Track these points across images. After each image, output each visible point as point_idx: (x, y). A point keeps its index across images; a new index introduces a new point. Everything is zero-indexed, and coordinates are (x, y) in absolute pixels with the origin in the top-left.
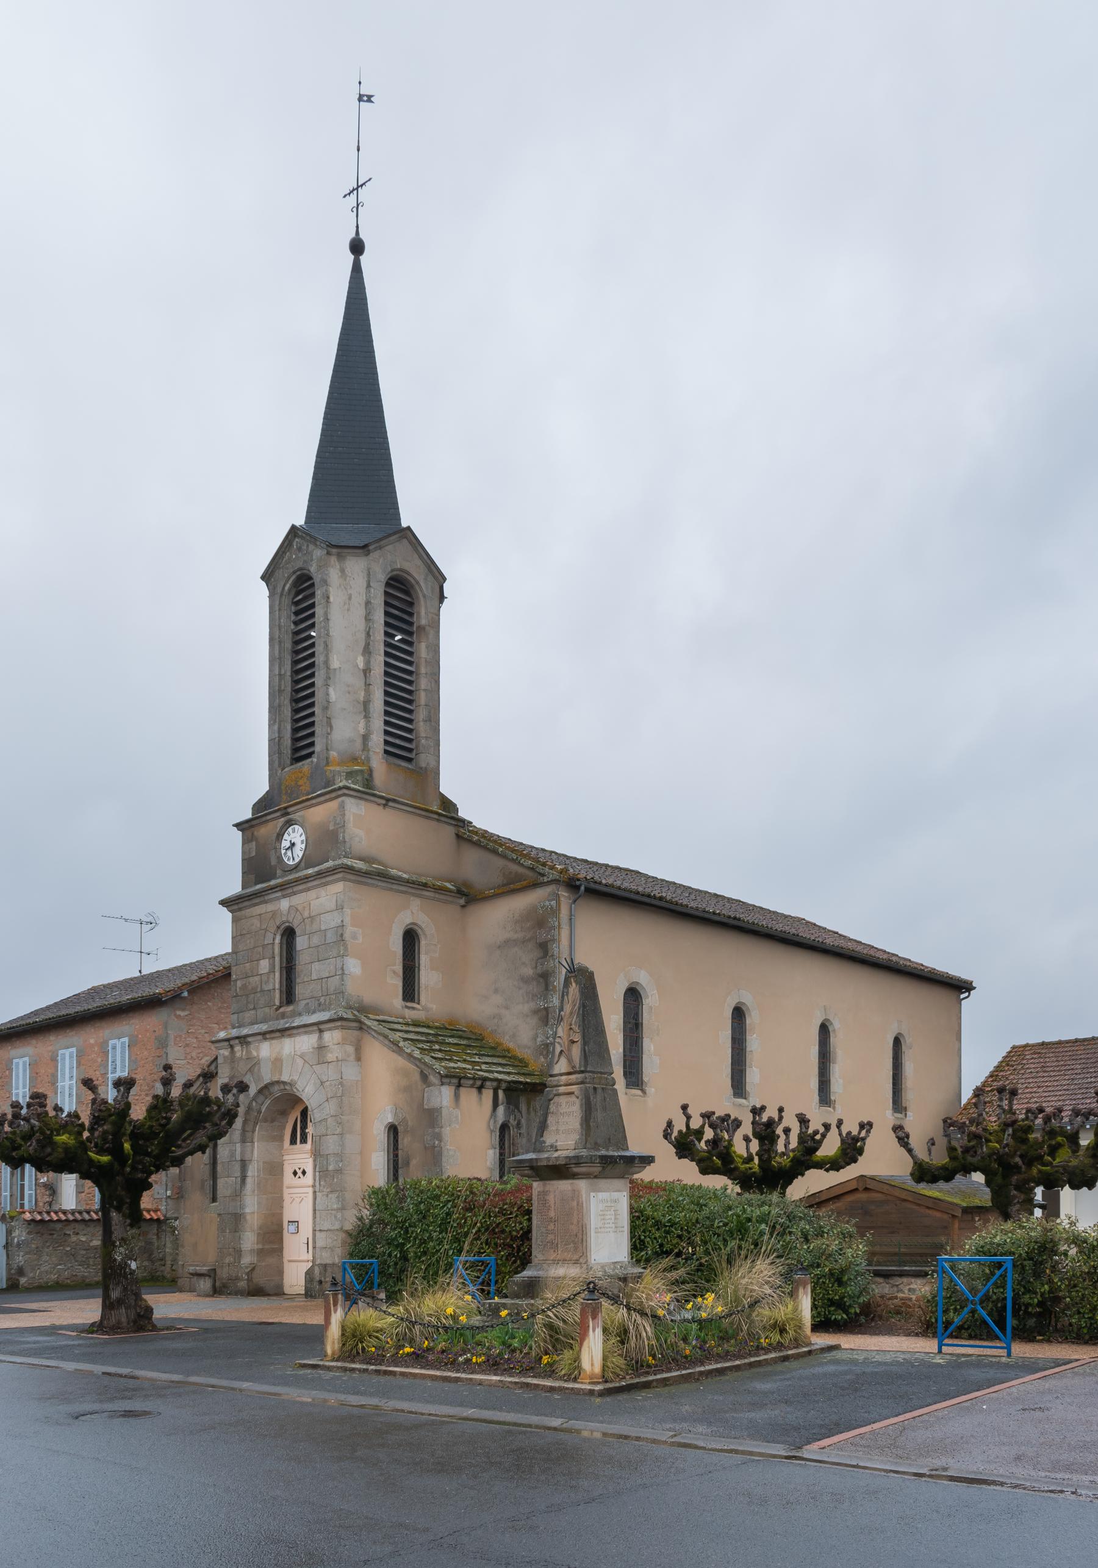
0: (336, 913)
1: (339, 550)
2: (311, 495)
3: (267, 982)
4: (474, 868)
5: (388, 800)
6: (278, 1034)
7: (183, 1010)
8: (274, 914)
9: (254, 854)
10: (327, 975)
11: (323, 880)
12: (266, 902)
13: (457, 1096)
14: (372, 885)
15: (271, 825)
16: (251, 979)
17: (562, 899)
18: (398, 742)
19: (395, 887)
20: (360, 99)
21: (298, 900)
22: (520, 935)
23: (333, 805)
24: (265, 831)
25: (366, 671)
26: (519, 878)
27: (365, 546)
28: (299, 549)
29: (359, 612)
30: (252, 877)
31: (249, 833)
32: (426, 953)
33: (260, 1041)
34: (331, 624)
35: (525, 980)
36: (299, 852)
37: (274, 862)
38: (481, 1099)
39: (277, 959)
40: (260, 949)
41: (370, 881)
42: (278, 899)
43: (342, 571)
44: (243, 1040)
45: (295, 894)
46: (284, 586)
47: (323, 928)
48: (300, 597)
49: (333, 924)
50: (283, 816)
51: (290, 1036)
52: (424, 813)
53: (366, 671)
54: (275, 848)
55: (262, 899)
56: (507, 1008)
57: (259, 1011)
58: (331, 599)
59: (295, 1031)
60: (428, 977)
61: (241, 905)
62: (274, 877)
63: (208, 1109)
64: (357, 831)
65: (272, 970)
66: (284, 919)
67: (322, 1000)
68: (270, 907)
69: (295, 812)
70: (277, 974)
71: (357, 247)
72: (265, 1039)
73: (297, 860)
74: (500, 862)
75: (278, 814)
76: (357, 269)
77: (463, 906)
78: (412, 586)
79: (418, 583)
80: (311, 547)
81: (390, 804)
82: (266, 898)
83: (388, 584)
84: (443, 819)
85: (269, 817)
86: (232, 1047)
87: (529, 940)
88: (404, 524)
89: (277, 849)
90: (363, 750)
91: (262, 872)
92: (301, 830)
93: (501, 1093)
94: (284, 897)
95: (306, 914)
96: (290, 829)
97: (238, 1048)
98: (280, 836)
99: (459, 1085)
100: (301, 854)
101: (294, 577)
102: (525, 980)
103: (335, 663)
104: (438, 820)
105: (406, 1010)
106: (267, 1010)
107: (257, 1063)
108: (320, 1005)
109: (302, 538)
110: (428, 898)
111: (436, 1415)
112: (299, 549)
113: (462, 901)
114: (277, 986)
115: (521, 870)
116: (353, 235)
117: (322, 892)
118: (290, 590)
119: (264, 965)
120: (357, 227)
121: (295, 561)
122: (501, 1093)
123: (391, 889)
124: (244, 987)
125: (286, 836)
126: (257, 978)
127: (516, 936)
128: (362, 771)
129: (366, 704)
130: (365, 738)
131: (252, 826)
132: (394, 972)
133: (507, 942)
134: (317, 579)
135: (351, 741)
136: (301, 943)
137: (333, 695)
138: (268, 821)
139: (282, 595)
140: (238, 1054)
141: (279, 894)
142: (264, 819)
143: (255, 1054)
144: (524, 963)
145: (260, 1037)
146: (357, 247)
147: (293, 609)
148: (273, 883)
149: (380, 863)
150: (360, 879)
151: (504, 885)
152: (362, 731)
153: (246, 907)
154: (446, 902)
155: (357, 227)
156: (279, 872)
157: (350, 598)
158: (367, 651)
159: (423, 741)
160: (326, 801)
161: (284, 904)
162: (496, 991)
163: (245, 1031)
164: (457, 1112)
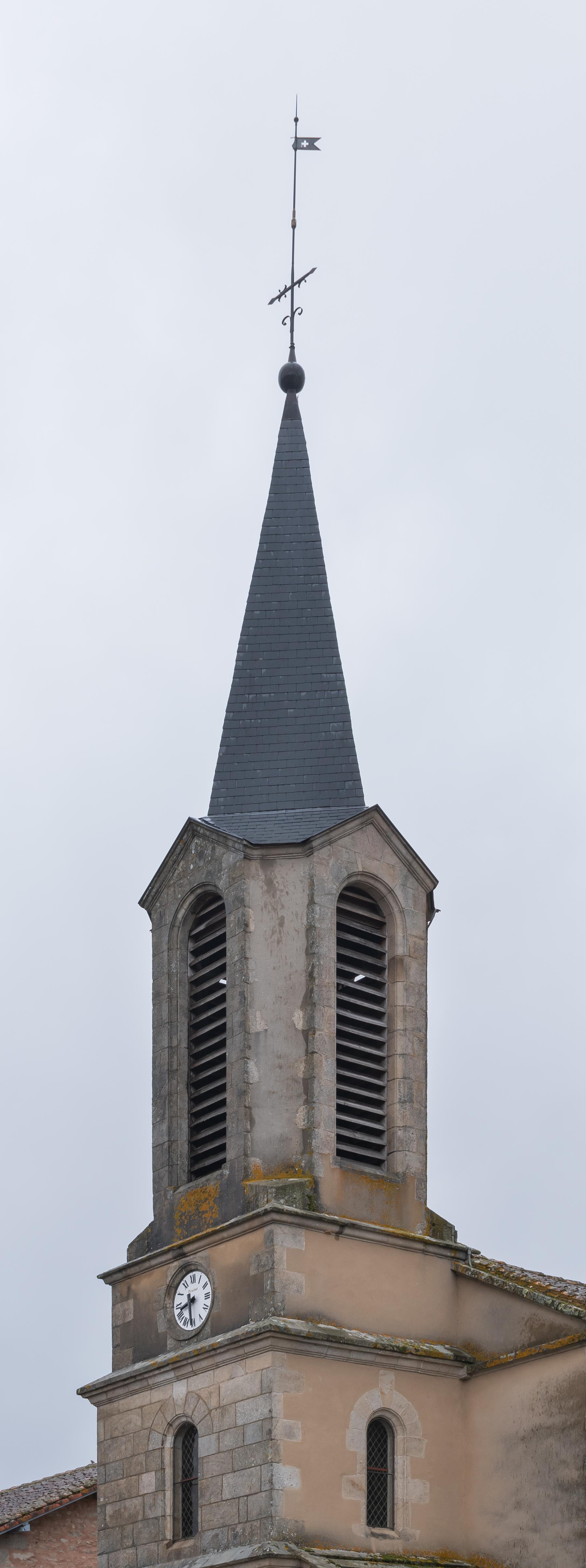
0: (260, 1400)
1: (264, 852)
3: (153, 1505)
4: (482, 1320)
5: (343, 1226)
7: (24, 1551)
8: (163, 1405)
9: (130, 1317)
10: (248, 1492)
11: (241, 1352)
12: (150, 1388)
15: (157, 1273)
16: (128, 1503)
18: (359, 1136)
19: (354, 1356)
20: (297, 146)
21: (200, 1383)
22: (557, 1420)
23: (257, 1238)
24: (148, 1284)
25: (308, 1033)
26: (556, 1332)
28: (200, 855)
29: (296, 944)
30: (129, 1352)
31: (123, 1287)
32: (405, 1453)
34: (251, 964)
35: (566, 1487)
36: (200, 1312)
37: (162, 1328)
39: (169, 1471)
40: (142, 1458)
41: (314, 1349)
42: (170, 1382)
43: (269, 883)
45: (195, 1373)
46: (177, 912)
47: (240, 1422)
48: (202, 927)
49: (256, 1416)
50: (176, 1258)
53: (308, 1033)
54: (165, 1308)
55: (144, 1383)
56: (535, 1530)
57: (140, 1550)
58: (252, 927)
60: (408, 1488)
61: (110, 1395)
62: (163, 1350)
65: (160, 1488)
66: (179, 1411)
67: (239, 1529)
68: (157, 1395)
69: (194, 1252)
70: (169, 1494)
71: (292, 379)
73: (198, 1323)
74: (525, 1311)
75: (169, 1256)
76: (291, 413)
77: (464, 1380)
78: (383, 897)
79: (391, 891)
80: (219, 850)
81: (347, 1231)
82: (151, 1382)
84: (431, 1249)
85: (154, 1262)
87: (573, 1426)
89: (167, 1309)
90: (303, 1153)
91: (142, 1341)
92: (204, 1279)
94: (178, 1379)
95: (213, 1403)
96: (188, 1278)
98: (172, 1289)
100: (204, 1314)
101: (192, 898)
102: (566, 1487)
103: (257, 1024)
104: (424, 1252)
105: (373, 1539)
106: (153, 1547)
108: (235, 1536)
109: (204, 837)
112: (200, 855)
113: (463, 1372)
114: (169, 1511)
115: (559, 1320)
116: (285, 361)
117: (239, 1369)
118: (185, 918)
119: (148, 1481)
120: (292, 347)
121: (193, 873)
123: (348, 1360)
124: (117, 1514)
125: (181, 1289)
126: (137, 1501)
127: (549, 1422)
128: (301, 1185)
129: (308, 1083)
130: (307, 1134)
132: (353, 1484)
133: (536, 1431)
134: (228, 899)
136: (205, 1445)
137: (255, 1072)
139: (173, 926)
141: (171, 1375)
144: (564, 1462)
146: (292, 379)
147: (191, 946)
148: (161, 1359)
149: (330, 1321)
151: (531, 1345)
152: (301, 1123)
153: (118, 1398)
154: (437, 1374)
155: (292, 347)
156: (170, 1343)
157: (281, 924)
158: (309, 1002)
159: (400, 1133)
160: (244, 1233)
161: (179, 1390)
162: (518, 1505)
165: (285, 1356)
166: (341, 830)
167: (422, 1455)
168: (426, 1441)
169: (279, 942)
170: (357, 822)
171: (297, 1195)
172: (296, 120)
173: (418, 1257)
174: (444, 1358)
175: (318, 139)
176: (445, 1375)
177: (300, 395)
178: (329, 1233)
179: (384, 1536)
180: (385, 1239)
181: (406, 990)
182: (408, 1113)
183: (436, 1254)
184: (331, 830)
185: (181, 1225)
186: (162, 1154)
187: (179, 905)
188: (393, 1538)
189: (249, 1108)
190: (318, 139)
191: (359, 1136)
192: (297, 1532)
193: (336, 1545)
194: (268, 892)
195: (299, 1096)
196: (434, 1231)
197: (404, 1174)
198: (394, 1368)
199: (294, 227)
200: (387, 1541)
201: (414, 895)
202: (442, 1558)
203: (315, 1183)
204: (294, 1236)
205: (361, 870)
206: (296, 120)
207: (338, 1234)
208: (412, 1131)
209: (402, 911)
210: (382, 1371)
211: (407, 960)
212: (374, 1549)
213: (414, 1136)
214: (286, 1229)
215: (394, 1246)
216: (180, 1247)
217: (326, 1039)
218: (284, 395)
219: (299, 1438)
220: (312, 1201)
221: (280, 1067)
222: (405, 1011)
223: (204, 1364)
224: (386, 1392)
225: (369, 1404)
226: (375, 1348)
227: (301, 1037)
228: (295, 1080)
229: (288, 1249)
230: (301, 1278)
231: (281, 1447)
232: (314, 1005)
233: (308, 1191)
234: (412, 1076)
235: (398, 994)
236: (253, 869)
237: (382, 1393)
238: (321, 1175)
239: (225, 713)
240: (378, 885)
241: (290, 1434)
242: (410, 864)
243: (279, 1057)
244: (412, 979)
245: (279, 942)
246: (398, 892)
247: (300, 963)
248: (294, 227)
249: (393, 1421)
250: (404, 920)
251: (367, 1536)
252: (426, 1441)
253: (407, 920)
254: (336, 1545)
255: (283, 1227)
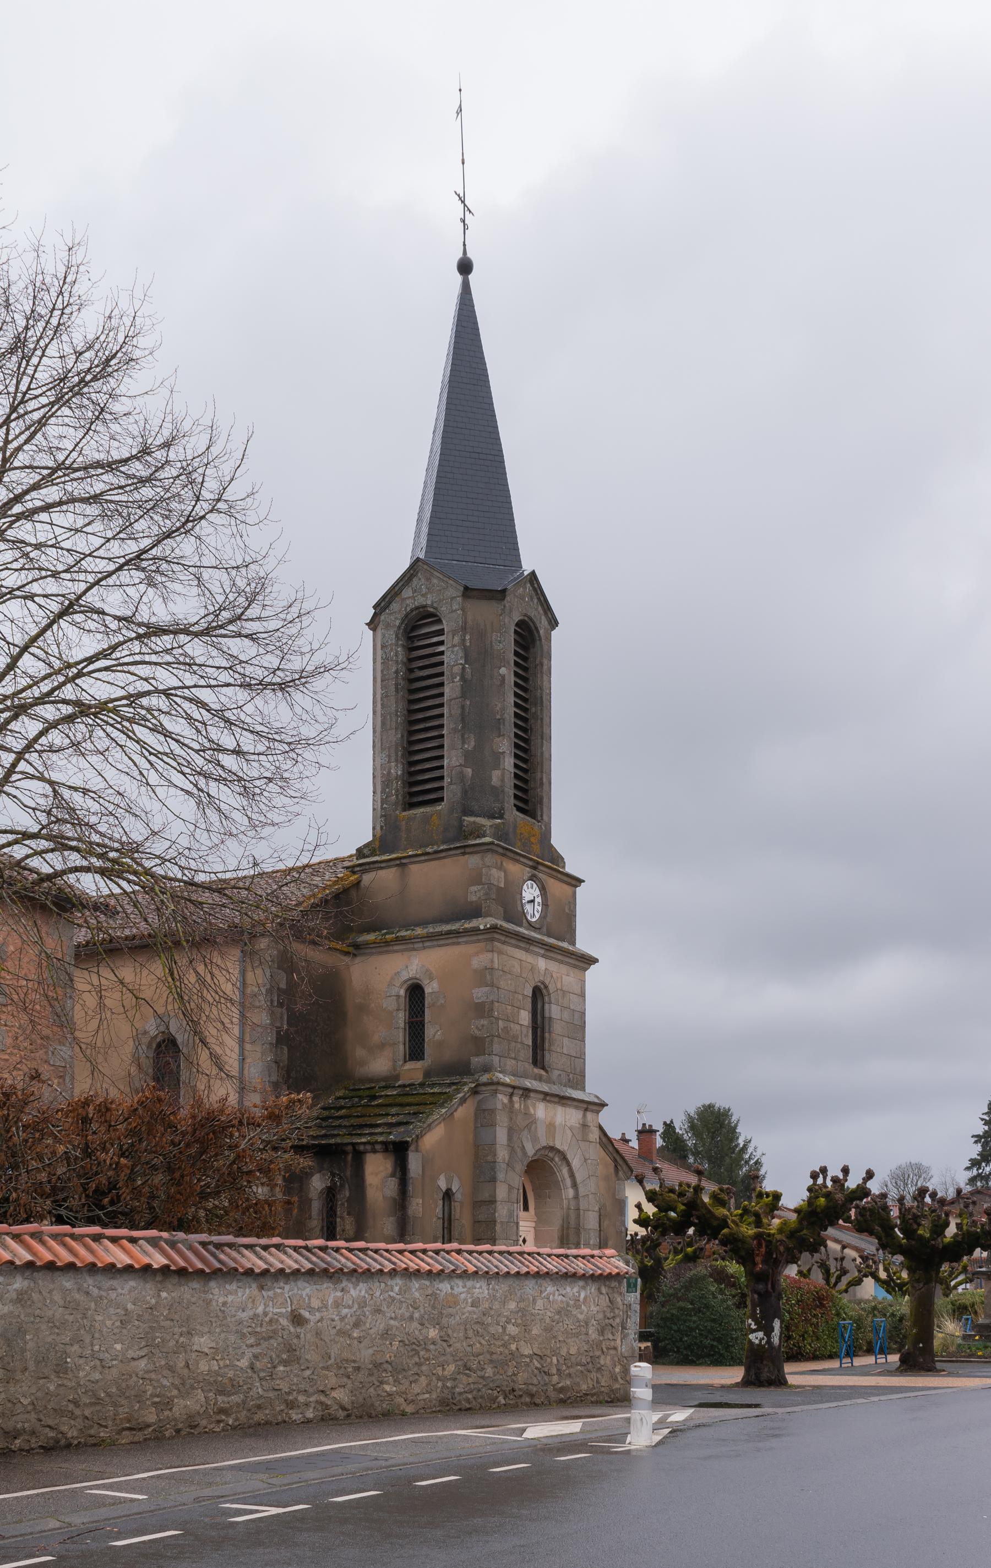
6: (556, 1100)
12: (527, 950)
19: (450, 941)
33: (538, 1100)
42: (537, 954)
44: (526, 1092)
51: (563, 1105)
52: (426, 858)
59: (570, 1103)
61: (507, 940)
63: (776, 1222)
71: (465, 267)
72: (544, 1099)
75: (531, 863)
82: (532, 948)
83: (517, 625)
85: (522, 859)
86: (511, 1095)
88: (527, 567)
94: (543, 956)
97: (516, 1099)
107: (534, 1121)
111: (244, 1493)
114: (401, 1039)
116: (461, 255)
120: (464, 245)
121: (411, 599)
124: (506, 1029)
131: (503, 855)
138: (518, 861)
140: (517, 1106)
141: (542, 952)
142: (518, 857)
143: (532, 1111)
145: (541, 1096)
146: (465, 267)
155: (464, 245)
161: (542, 964)
163: (528, 1083)
185: (520, 840)
186: (383, 782)
187: (395, 615)
199: (463, 163)
216: (538, 863)
218: (459, 278)
223: (560, 957)
235: (395, 736)
248: (463, 163)
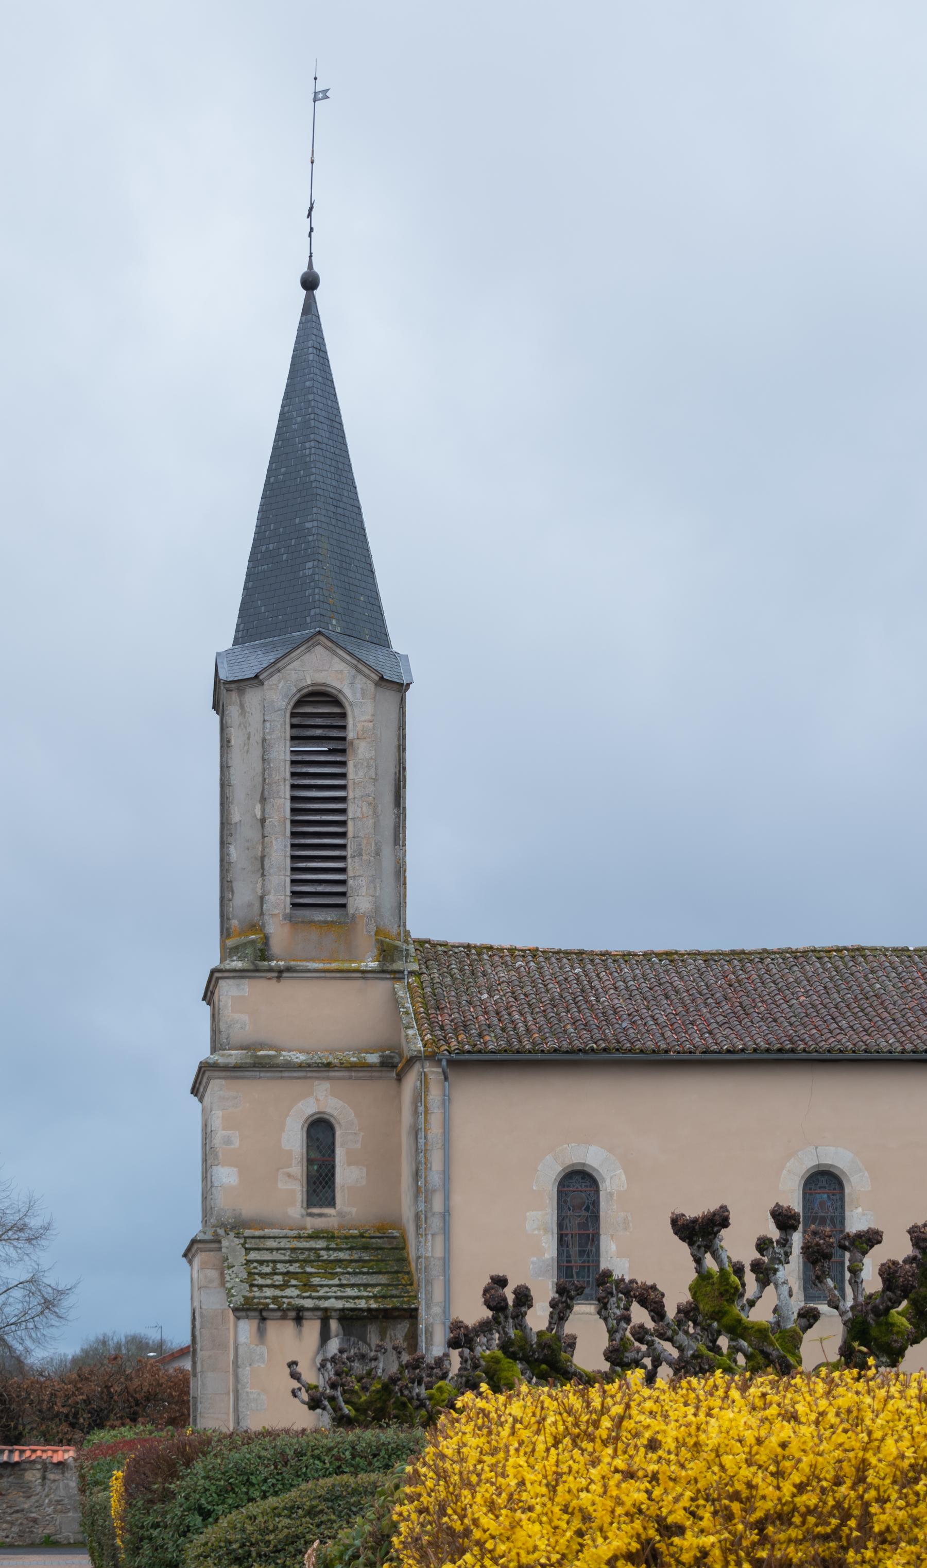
2: (241, 610)
13: (261, 1332)
14: (255, 1078)
17: (431, 1076)
18: (320, 889)
19: (286, 1074)
27: (257, 677)
32: (342, 1146)
38: (300, 1332)
41: (247, 1074)
43: (242, 706)
58: (233, 742)
60: (346, 1175)
64: (236, 1016)
71: (310, 282)
76: (309, 309)
79: (340, 691)
81: (285, 975)
84: (369, 975)
93: (334, 1325)
99: (263, 1319)
104: (363, 978)
105: (308, 1219)
110: (339, 1079)
116: (305, 269)
122: (334, 1325)
123: (282, 1078)
128: (253, 942)
132: (289, 1175)
135: (250, 905)
146: (310, 282)
149: (271, 1048)
150: (228, 1074)
152: (260, 893)
154: (371, 1078)
155: (311, 256)
157: (249, 738)
164: (264, 1349)
165: (223, 1082)
166: (286, 659)
167: (359, 1146)
168: (362, 1134)
169: (247, 752)
170: (303, 648)
171: (249, 951)
172: (315, 79)
173: (359, 984)
174: (370, 1066)
175: (328, 90)
176: (380, 1078)
177: (317, 293)
178: (269, 979)
179: (320, 1215)
180: (323, 975)
181: (355, 766)
182: (357, 865)
183: (377, 978)
184: (275, 663)
188: (330, 1216)
189: (231, 882)
190: (328, 90)
191: (320, 889)
192: (235, 1218)
193: (271, 1225)
194: (241, 714)
195: (258, 871)
196: (384, 956)
197: (353, 915)
198: (328, 1078)
199: (312, 162)
200: (323, 1219)
201: (362, 689)
202: (378, 1230)
203: (266, 939)
204: (238, 985)
205: (309, 682)
206: (315, 79)
207: (279, 978)
208: (361, 878)
209: (351, 704)
210: (316, 1082)
211: (356, 742)
212: (309, 1226)
213: (364, 883)
214: (231, 982)
215: (335, 978)
217: (276, 824)
219: (237, 1144)
220: (264, 954)
221: (248, 849)
222: (354, 783)
224: (321, 1098)
225: (308, 1108)
226: (300, 1066)
227: (259, 824)
228: (256, 859)
229: (233, 997)
230: (245, 1018)
231: (220, 1154)
232: (265, 799)
233: (259, 946)
234: (361, 834)
236: (234, 698)
237: (317, 1100)
238: (272, 931)
239: (247, 563)
240: (330, 689)
241: (228, 1141)
242: (356, 666)
243: (248, 841)
244: (361, 756)
245: (247, 752)
246: (347, 691)
247: (258, 766)
248: (312, 162)
249: (332, 1120)
250: (353, 711)
251: (303, 1216)
252: (362, 1134)
253: (355, 710)
254: (271, 1225)
255: (227, 981)
